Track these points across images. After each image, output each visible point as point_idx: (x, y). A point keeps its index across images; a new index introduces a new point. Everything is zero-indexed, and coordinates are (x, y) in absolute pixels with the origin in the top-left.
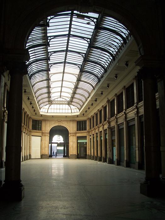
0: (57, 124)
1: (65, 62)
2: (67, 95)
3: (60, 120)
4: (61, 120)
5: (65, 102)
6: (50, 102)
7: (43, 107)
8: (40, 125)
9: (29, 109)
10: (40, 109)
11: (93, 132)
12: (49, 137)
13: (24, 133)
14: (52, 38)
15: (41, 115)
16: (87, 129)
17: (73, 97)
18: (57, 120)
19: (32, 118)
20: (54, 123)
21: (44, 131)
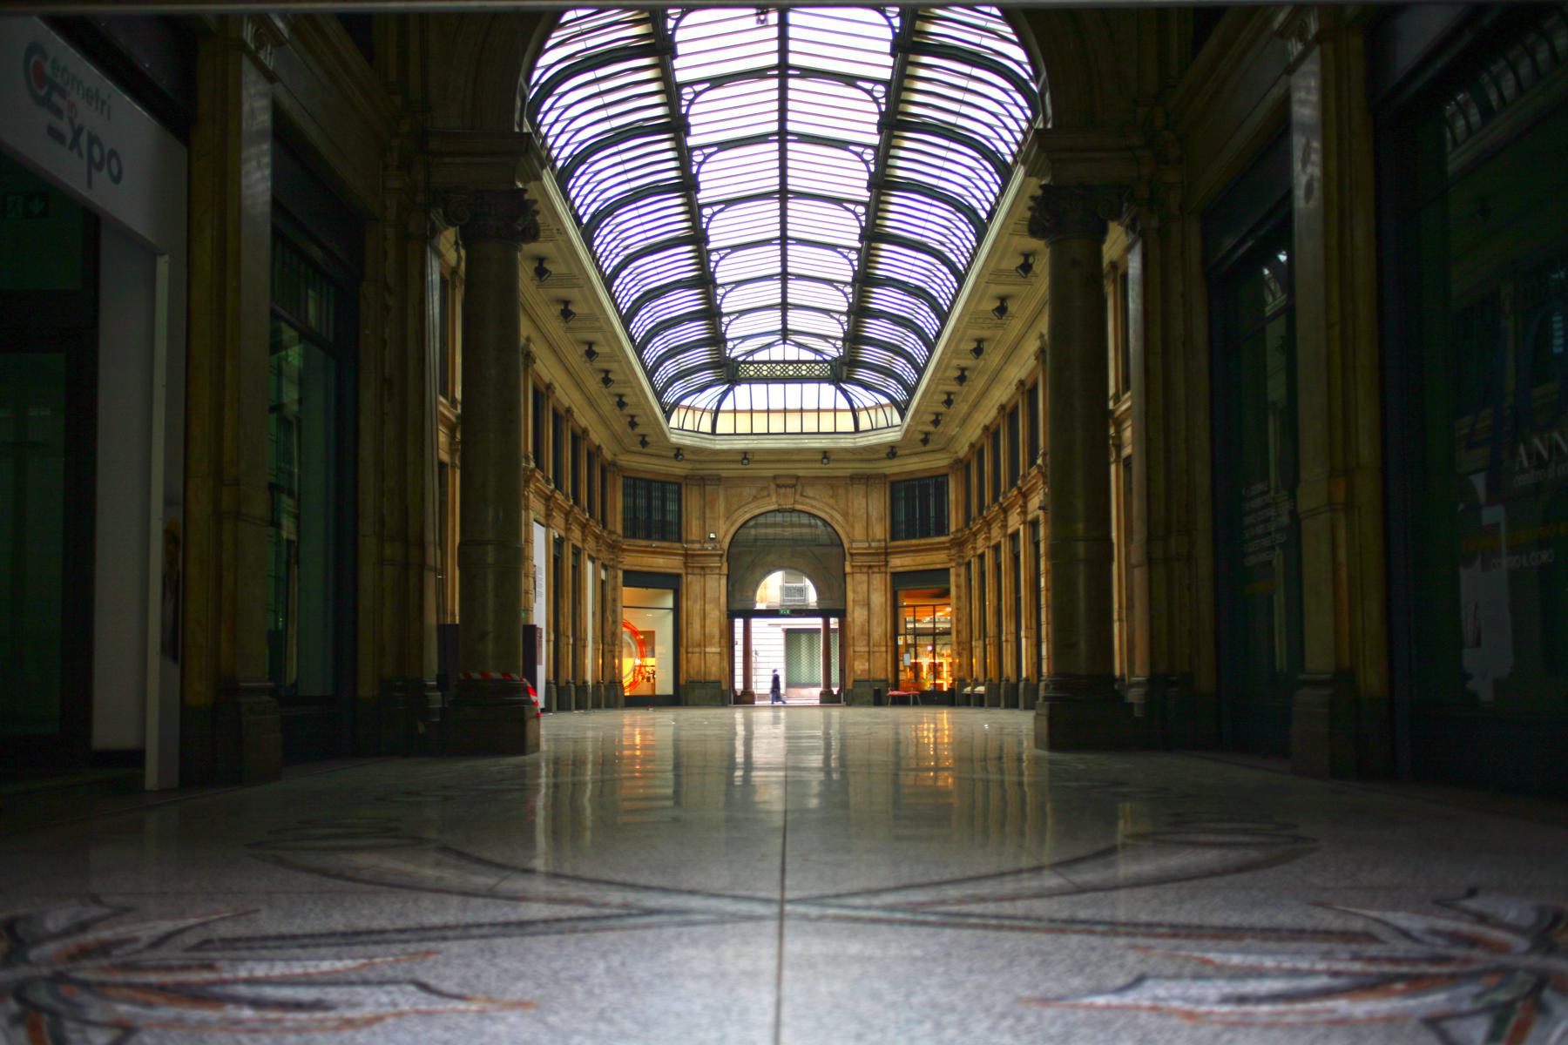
1: (783, 135)
2: (823, 327)
4: (798, 478)
6: (730, 373)
7: (686, 402)
10: (668, 419)
11: (981, 545)
13: (593, 559)
14: (716, 208)
15: (679, 452)
16: (953, 528)
17: (854, 338)
18: (775, 478)
19: (621, 469)
20: (755, 498)
21: (697, 546)
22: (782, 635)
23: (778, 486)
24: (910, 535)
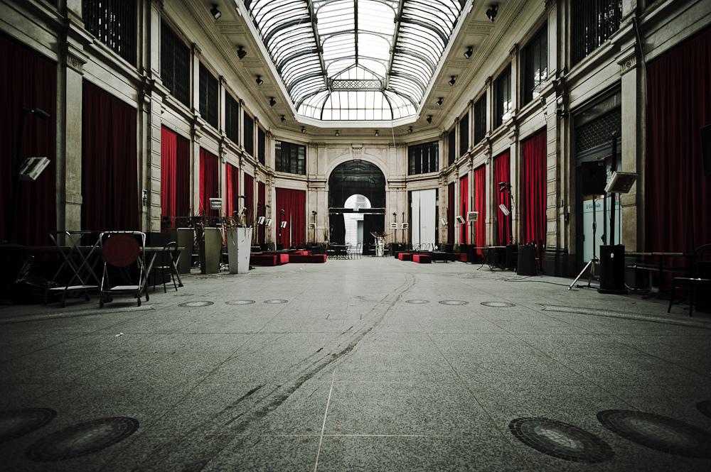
0: (349, 156)
3: (360, 144)
5: (374, 85)
7: (306, 102)
8: (301, 157)
9: (250, 91)
10: (297, 109)
12: (327, 194)
15: (303, 128)
20: (342, 154)
22: (356, 223)
23: (353, 148)
24: (418, 172)
